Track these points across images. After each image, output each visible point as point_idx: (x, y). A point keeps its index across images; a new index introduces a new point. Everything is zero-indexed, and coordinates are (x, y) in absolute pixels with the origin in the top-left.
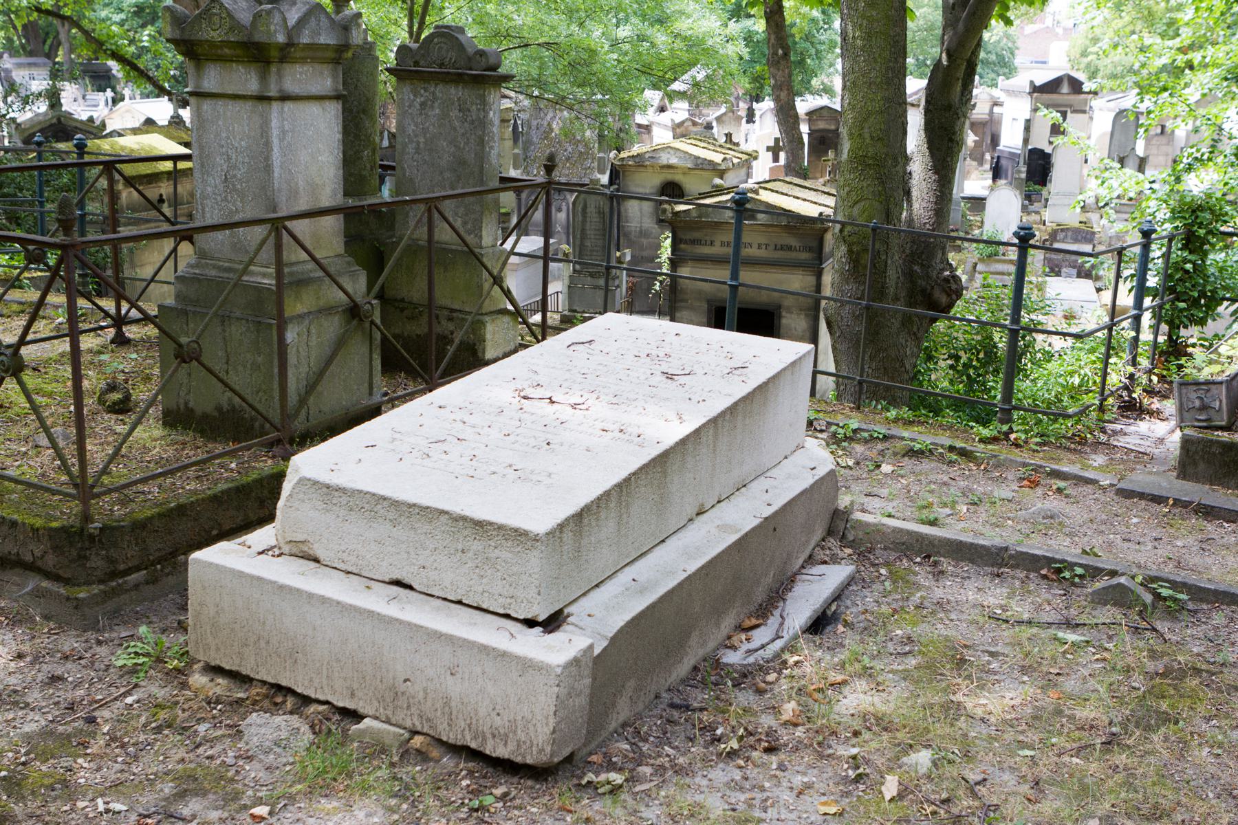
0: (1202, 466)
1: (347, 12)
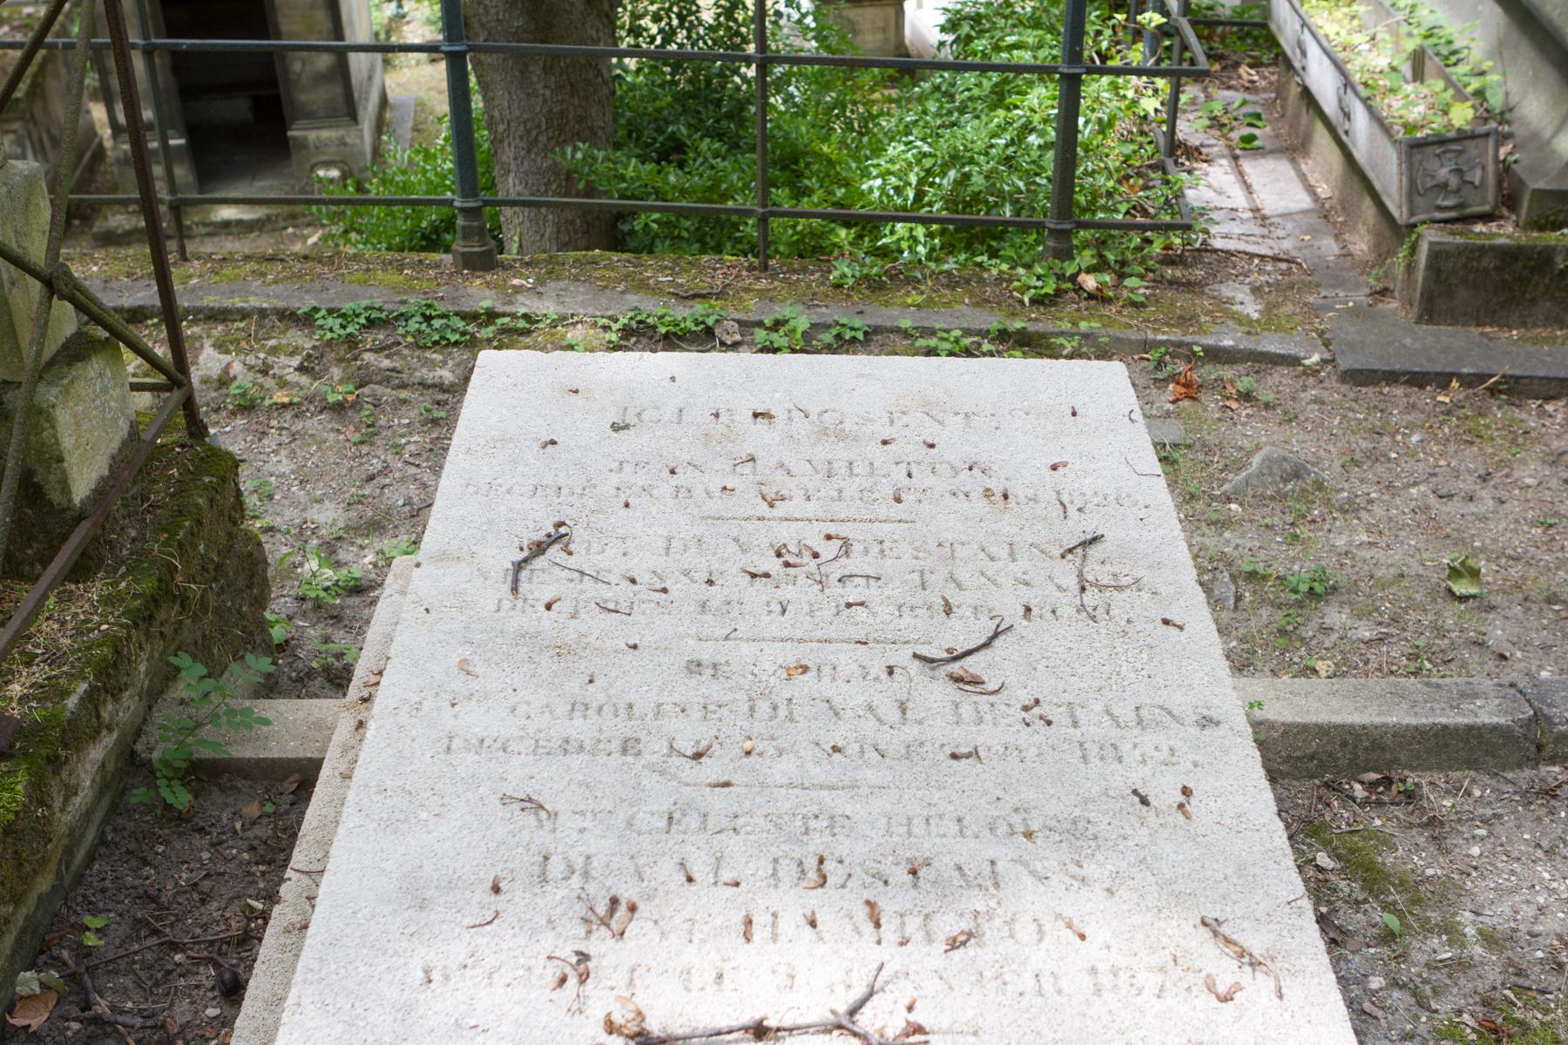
0: (1463, 294)
1: (131, 327)
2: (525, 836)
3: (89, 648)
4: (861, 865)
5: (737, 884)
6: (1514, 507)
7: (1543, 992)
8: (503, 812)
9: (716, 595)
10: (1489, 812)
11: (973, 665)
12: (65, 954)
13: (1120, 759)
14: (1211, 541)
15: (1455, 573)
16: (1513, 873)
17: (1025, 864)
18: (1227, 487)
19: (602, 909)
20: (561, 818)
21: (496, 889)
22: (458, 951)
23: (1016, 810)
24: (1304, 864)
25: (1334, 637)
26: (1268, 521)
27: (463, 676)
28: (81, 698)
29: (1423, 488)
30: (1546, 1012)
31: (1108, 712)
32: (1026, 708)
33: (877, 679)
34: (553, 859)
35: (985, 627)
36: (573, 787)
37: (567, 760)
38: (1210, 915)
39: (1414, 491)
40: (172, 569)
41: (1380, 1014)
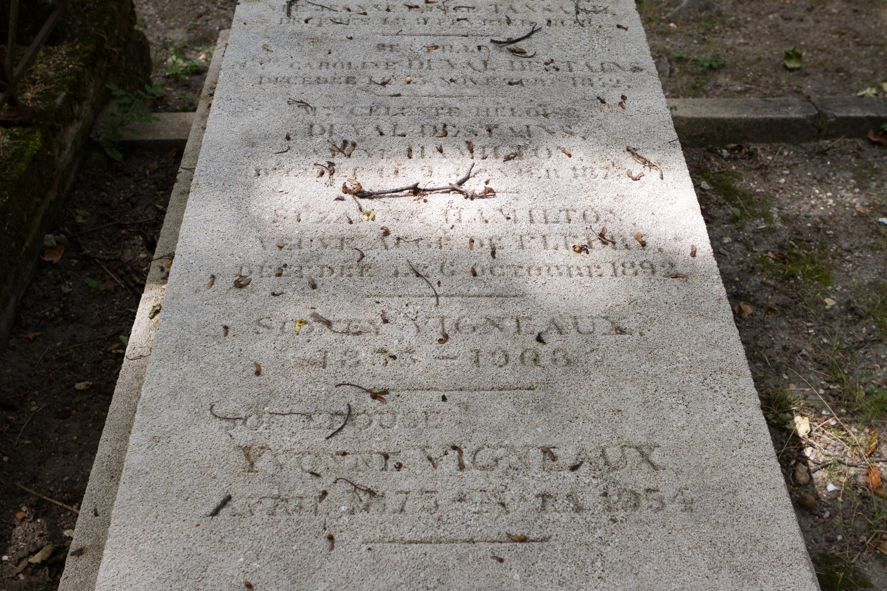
2: (301, 117)
3: (64, 76)
4: (464, 127)
5: (404, 136)
6: (825, 25)
7: (809, 241)
8: (288, 107)
9: (391, 16)
10: (791, 162)
11: (519, 45)
12: (66, 229)
13: (592, 85)
14: (658, 43)
15: (788, 56)
16: (800, 190)
17: (544, 127)
18: (669, 14)
19: (339, 145)
20: (318, 110)
21: (288, 138)
22: (272, 163)
23: (540, 106)
24: (697, 187)
25: (721, 89)
26: (690, 32)
27: (265, 52)
28: (63, 99)
29: (776, 15)
30: (810, 250)
31: (587, 65)
32: (546, 64)
33: (473, 51)
34: (315, 126)
35: (528, 28)
36: (323, 97)
37: (320, 86)
38: (633, 145)
39: (771, 16)
40: (103, 41)
41: (727, 253)
